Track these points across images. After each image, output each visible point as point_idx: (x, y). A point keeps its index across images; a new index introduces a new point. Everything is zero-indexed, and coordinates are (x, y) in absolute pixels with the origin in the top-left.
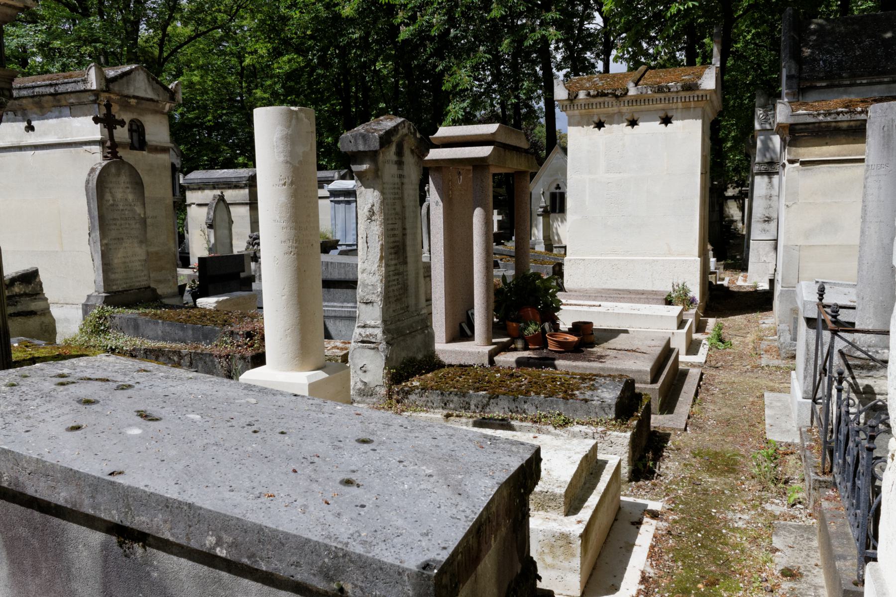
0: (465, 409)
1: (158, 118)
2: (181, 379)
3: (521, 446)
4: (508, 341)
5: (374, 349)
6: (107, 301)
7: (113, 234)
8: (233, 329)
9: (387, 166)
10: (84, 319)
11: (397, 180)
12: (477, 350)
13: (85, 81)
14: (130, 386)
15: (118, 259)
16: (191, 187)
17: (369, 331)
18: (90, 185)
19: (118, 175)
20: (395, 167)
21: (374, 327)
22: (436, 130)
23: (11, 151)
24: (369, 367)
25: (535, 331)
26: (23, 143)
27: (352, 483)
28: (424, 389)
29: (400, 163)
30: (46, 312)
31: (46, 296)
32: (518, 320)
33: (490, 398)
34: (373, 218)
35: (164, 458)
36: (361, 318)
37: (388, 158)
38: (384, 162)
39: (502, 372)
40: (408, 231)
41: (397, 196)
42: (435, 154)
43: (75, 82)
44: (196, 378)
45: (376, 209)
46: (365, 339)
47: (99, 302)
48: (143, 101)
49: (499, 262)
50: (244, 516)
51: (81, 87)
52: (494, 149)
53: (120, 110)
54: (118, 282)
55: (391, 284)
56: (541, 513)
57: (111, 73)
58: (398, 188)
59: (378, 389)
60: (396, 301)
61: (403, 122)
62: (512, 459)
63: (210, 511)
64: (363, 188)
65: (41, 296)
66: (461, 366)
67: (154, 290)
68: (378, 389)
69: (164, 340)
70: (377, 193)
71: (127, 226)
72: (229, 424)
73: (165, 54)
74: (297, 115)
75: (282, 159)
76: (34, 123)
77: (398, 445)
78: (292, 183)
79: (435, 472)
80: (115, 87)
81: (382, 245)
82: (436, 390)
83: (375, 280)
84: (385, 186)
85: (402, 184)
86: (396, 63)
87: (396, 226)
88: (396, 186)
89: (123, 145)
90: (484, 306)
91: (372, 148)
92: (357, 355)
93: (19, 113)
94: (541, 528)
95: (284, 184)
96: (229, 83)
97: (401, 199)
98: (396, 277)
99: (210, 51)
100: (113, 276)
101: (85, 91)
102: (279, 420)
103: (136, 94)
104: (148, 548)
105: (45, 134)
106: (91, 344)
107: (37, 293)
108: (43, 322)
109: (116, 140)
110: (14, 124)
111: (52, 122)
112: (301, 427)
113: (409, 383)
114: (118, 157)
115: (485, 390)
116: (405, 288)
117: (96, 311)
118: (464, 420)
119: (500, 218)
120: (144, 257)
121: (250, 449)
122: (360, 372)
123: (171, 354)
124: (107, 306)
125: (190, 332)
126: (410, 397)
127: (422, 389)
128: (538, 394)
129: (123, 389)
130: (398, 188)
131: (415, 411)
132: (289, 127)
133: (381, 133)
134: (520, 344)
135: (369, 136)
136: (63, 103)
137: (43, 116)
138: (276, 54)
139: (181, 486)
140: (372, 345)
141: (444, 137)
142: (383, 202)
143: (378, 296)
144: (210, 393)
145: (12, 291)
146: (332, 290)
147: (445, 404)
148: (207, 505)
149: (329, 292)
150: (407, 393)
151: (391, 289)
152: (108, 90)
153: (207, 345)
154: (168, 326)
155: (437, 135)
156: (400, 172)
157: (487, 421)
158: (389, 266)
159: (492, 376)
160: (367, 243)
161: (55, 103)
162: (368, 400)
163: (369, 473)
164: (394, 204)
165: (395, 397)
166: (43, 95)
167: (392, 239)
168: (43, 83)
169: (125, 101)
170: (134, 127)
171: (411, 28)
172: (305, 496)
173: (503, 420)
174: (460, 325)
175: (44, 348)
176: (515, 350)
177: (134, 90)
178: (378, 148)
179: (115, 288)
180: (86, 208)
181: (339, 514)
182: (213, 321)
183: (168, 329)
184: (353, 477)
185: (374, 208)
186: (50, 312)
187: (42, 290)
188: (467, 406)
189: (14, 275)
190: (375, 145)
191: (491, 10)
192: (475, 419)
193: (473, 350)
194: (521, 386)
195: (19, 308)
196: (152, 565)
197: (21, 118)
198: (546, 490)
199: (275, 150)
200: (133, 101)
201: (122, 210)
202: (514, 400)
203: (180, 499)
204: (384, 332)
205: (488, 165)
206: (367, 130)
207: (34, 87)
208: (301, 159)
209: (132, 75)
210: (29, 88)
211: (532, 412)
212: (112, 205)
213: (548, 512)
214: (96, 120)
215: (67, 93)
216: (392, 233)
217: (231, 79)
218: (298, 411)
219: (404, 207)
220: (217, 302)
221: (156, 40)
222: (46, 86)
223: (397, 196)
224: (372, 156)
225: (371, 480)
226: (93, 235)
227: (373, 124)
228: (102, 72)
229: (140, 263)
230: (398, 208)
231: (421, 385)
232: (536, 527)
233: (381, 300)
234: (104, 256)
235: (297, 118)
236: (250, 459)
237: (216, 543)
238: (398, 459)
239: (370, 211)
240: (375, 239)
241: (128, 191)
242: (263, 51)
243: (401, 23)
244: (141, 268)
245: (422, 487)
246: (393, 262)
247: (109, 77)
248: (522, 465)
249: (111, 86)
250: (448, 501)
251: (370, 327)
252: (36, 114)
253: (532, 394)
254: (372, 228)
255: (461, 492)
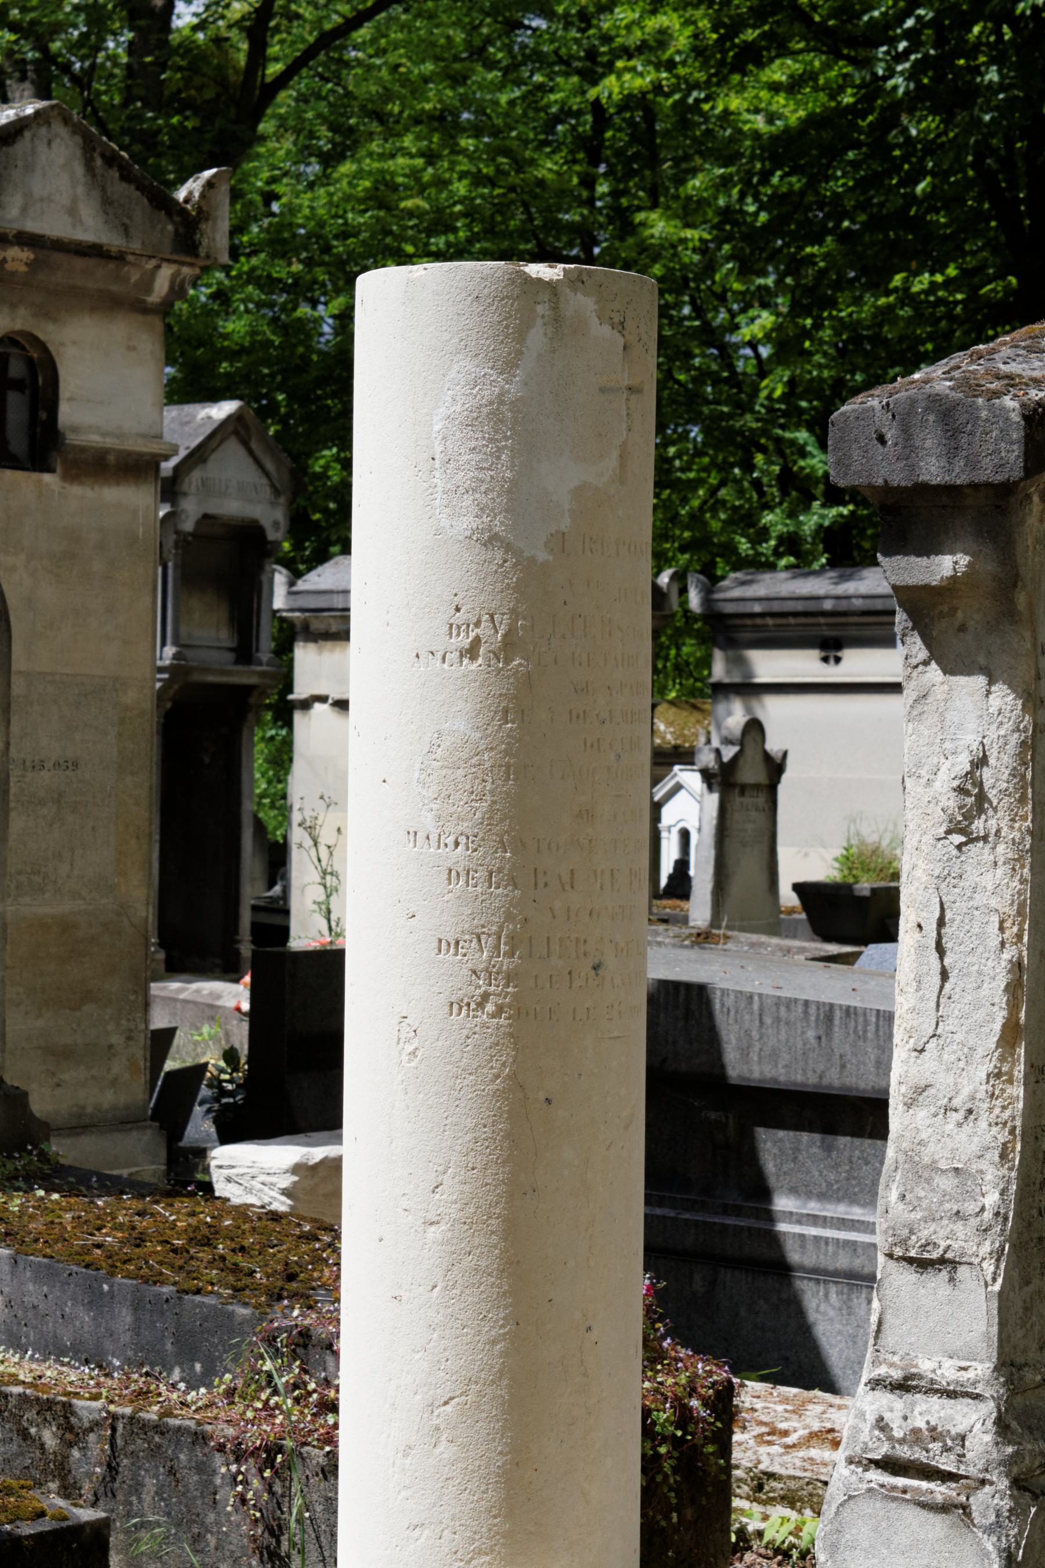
5: (944, 1508)
8: (310, 1320)
16: (316, 626)
21: (951, 1395)
23: (250, 460)
34: (978, 826)
46: (904, 1452)
64: (934, 672)
73: (274, 69)
75: (466, 523)
78: (509, 646)
81: (1017, 966)
83: (974, 1148)
91: (986, 473)
95: (471, 652)
99: (478, 53)
103: (31, 226)
123: (31, 1414)
125: (125, 1317)
132: (509, 365)
135: (973, 409)
140: (940, 1491)
146: (843, 1141)
149: (828, 1149)
153: (192, 1387)
154: (37, 1279)
177: (24, 209)
178: (1017, 474)
183: (33, 1291)
185: (986, 775)
204: (1002, 1427)
206: (969, 386)
208: (566, 523)
220: (297, 1169)
227: (1006, 352)
235: (557, 320)
239: (961, 790)
240: (982, 936)
251: (934, 1390)
254: (972, 876)
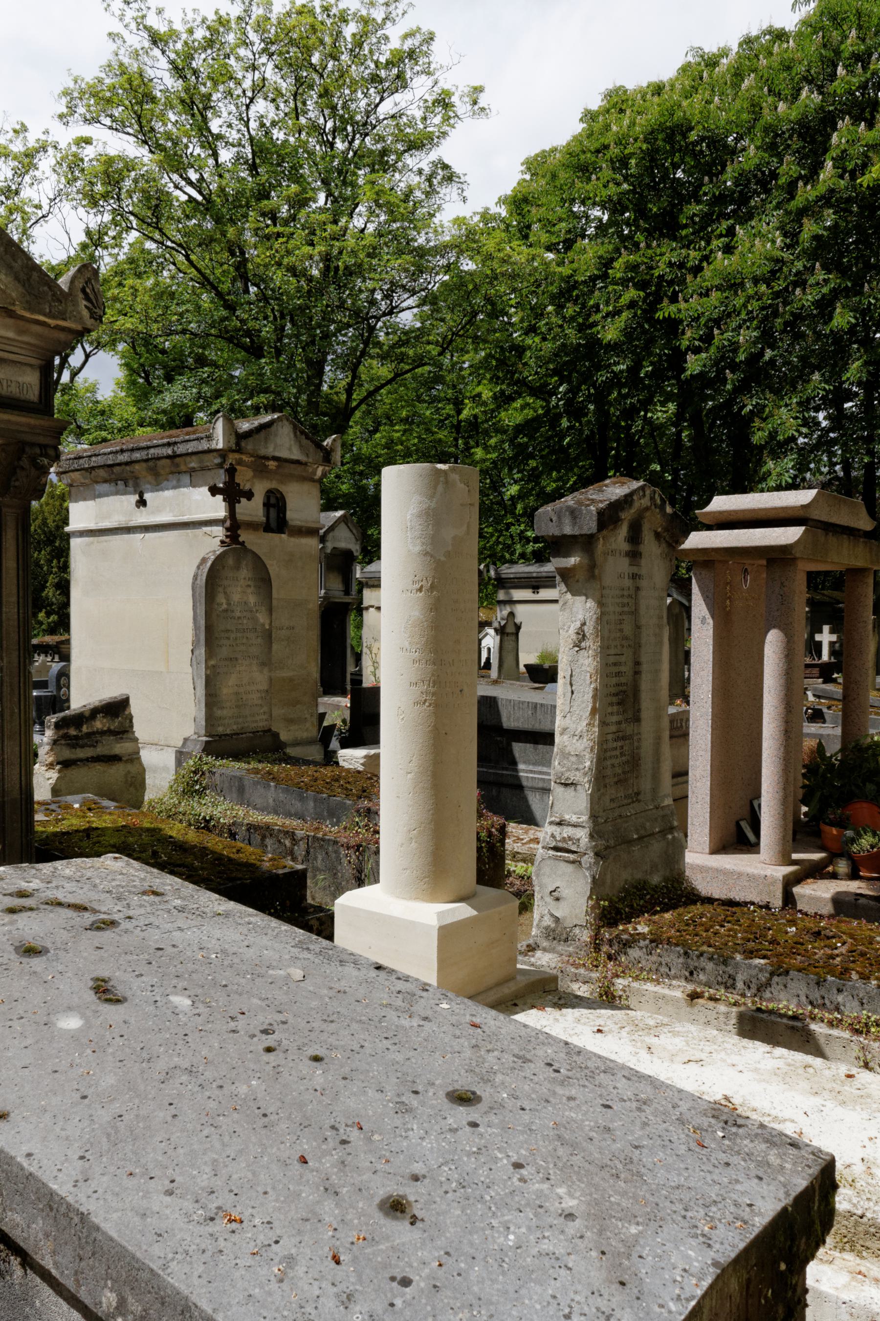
0: (726, 988)
1: (306, 487)
2: (203, 914)
3: (792, 1151)
4: (822, 859)
5: (573, 862)
6: (208, 749)
7: (224, 652)
9: (611, 559)
10: (176, 771)
11: (627, 583)
12: (763, 873)
13: (209, 438)
14: (113, 923)
15: (227, 689)
17: (567, 832)
18: (198, 582)
19: (237, 568)
20: (626, 561)
21: (575, 826)
22: (708, 502)
24: (565, 892)
25: (872, 847)
26: (132, 524)
27: (403, 1212)
28: (656, 940)
29: (634, 555)
30: (134, 758)
31: (137, 734)
32: (842, 824)
33: (772, 974)
34: (583, 644)
35: (89, 1092)
36: (555, 809)
37: (614, 546)
38: (606, 554)
39: (801, 924)
40: (645, 667)
41: (626, 609)
42: (697, 540)
43: (197, 439)
44: (227, 915)
45: (589, 629)
46: (560, 845)
47: (196, 749)
48: (287, 464)
49: (825, 710)
50: (165, 1267)
51: (204, 445)
52: (805, 532)
53: (254, 476)
54: (226, 721)
55: (608, 754)
56: (849, 1256)
57: (245, 426)
58: (630, 596)
59: (577, 931)
60: (616, 783)
61: (642, 488)
62: (764, 1188)
63: (111, 1239)
65: (130, 736)
66: (730, 903)
67: (276, 735)
68: (577, 931)
69: (276, 813)
70: (591, 604)
71: (244, 641)
72: (232, 1025)
73: (354, 404)
74: (446, 478)
75: (418, 548)
76: (147, 496)
77: (526, 1117)
78: (432, 587)
79: (583, 1207)
80: (248, 445)
81: (596, 689)
82: (677, 945)
83: (582, 747)
84: (604, 592)
85: (638, 589)
86: (418, 329)
87: (623, 659)
88: (626, 593)
89: (252, 526)
90: (779, 796)
91: (585, 531)
92: (546, 870)
93: (131, 483)
94: (845, 1297)
95: (420, 590)
96: (440, 440)
97: (635, 613)
98: (619, 744)
100: (219, 713)
101: (210, 451)
102: (324, 1026)
103: (277, 454)
104: (29, 1271)
105: (158, 510)
106: (181, 809)
107: (125, 731)
108: (129, 772)
109: (239, 517)
110: (123, 497)
111: (168, 493)
112: (356, 1047)
113: (630, 927)
114: (238, 543)
115: (764, 957)
116: (634, 762)
117: (191, 762)
118: (722, 1008)
119: (834, 638)
120: (264, 686)
121: (243, 1089)
122: (549, 899)
124: (207, 755)
126: (630, 951)
127: (652, 941)
128: (865, 977)
129: (99, 929)
130: (630, 596)
131: (637, 978)
132: (431, 497)
133: (601, 505)
134: (842, 867)
135: (581, 510)
136: (183, 468)
137: (157, 487)
138: (503, 400)
139: (87, 1165)
140: (572, 857)
141: (720, 513)
142: (601, 619)
143: (585, 774)
144: (235, 949)
145: (92, 726)
146: (540, 746)
147: (691, 973)
148: (109, 1228)
149: (536, 749)
150: (626, 945)
151: (609, 763)
152: (239, 450)
153: (333, 826)
155: (708, 509)
156: (635, 569)
157: (764, 1016)
158: (608, 725)
159: (780, 930)
160: (571, 685)
161: (173, 469)
162: (561, 948)
163: (445, 1188)
164: (621, 622)
165: (605, 948)
166: (159, 458)
167: (614, 680)
168: (160, 442)
169: (260, 464)
170: (273, 501)
171: (704, 355)
172: (299, 1232)
173: (795, 1018)
174: (738, 825)
175: (110, 814)
176: (834, 876)
178: (595, 531)
179: (220, 730)
180: (191, 613)
181: (349, 1297)
182: (347, 789)
183: (282, 796)
184: (411, 1193)
186: (139, 758)
187: (132, 726)
188: (730, 982)
189: (97, 704)
190: (590, 525)
191: (831, 318)
192: (742, 1008)
193: (756, 872)
194: (833, 957)
195: (100, 750)
196: (32, 1305)
197: (131, 489)
198: (859, 1212)
199: (409, 534)
200: (272, 464)
201: (239, 618)
202: (818, 984)
203: (70, 1199)
204: (591, 836)
205: (795, 559)
206: (580, 503)
207: (148, 448)
208: (450, 548)
209: (274, 428)
210: (143, 448)
211: (852, 1010)
212: (226, 611)
213: (862, 1258)
214: (214, 491)
215: (187, 454)
216: (615, 669)
217: (442, 435)
218: (367, 1006)
219: (638, 627)
220: (366, 757)
221: (344, 383)
222: (163, 445)
223: (626, 609)
224: (586, 543)
225: (444, 1207)
226: (197, 652)
228: (233, 425)
229: (259, 695)
230: (628, 629)
231: (650, 932)
232: (831, 1291)
233: (590, 782)
234: (209, 682)
235: (447, 482)
236: (236, 1116)
237: (117, 1308)
238: (514, 1158)
240: (584, 680)
241: (249, 590)
242: (487, 394)
243: (688, 348)
244: (260, 702)
245: (545, 1246)
246: (614, 719)
247: (240, 431)
248: (784, 1210)
249: (243, 444)
250: (591, 1301)
252: (150, 483)
253: (854, 976)
254: (581, 661)
255: (625, 1278)
